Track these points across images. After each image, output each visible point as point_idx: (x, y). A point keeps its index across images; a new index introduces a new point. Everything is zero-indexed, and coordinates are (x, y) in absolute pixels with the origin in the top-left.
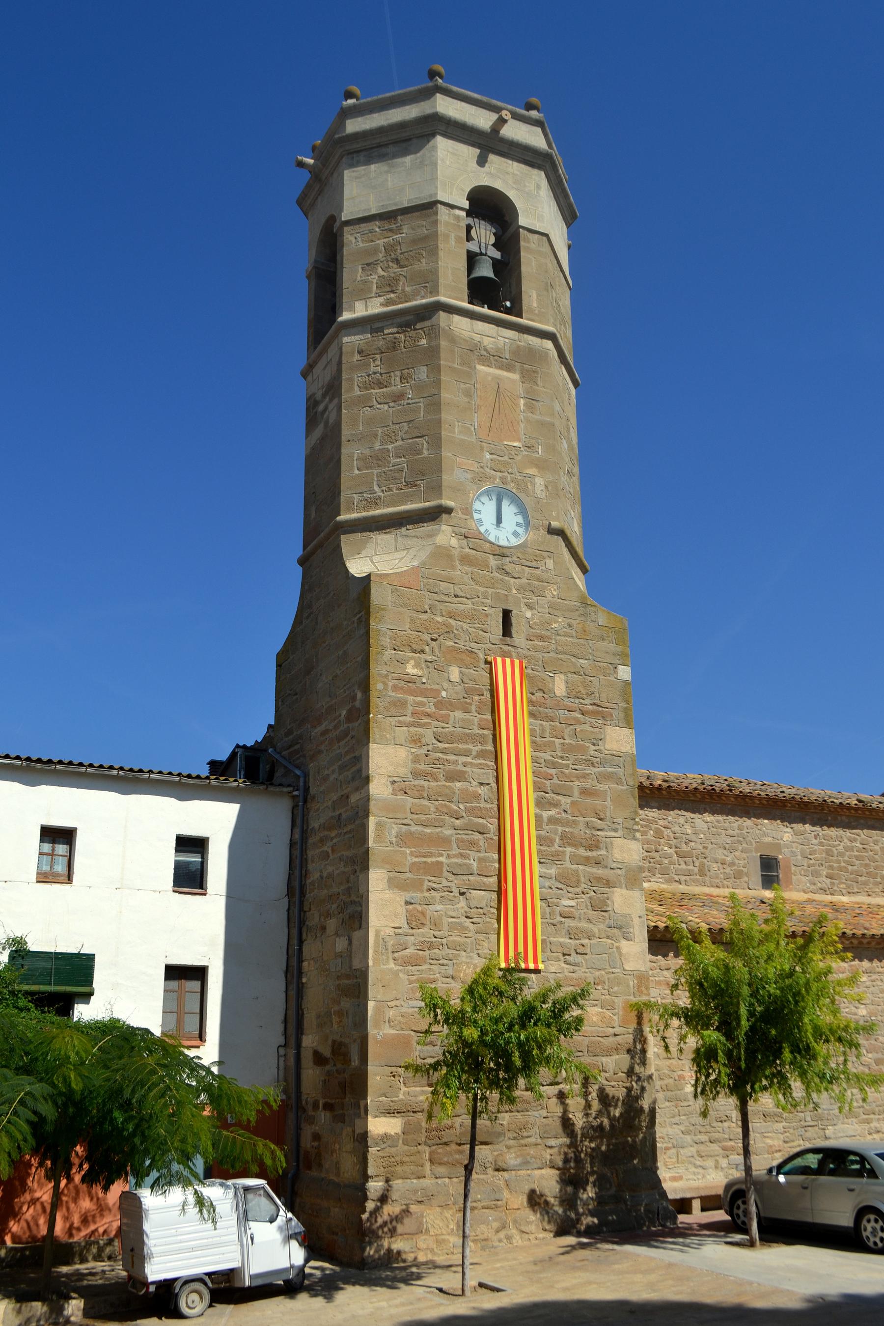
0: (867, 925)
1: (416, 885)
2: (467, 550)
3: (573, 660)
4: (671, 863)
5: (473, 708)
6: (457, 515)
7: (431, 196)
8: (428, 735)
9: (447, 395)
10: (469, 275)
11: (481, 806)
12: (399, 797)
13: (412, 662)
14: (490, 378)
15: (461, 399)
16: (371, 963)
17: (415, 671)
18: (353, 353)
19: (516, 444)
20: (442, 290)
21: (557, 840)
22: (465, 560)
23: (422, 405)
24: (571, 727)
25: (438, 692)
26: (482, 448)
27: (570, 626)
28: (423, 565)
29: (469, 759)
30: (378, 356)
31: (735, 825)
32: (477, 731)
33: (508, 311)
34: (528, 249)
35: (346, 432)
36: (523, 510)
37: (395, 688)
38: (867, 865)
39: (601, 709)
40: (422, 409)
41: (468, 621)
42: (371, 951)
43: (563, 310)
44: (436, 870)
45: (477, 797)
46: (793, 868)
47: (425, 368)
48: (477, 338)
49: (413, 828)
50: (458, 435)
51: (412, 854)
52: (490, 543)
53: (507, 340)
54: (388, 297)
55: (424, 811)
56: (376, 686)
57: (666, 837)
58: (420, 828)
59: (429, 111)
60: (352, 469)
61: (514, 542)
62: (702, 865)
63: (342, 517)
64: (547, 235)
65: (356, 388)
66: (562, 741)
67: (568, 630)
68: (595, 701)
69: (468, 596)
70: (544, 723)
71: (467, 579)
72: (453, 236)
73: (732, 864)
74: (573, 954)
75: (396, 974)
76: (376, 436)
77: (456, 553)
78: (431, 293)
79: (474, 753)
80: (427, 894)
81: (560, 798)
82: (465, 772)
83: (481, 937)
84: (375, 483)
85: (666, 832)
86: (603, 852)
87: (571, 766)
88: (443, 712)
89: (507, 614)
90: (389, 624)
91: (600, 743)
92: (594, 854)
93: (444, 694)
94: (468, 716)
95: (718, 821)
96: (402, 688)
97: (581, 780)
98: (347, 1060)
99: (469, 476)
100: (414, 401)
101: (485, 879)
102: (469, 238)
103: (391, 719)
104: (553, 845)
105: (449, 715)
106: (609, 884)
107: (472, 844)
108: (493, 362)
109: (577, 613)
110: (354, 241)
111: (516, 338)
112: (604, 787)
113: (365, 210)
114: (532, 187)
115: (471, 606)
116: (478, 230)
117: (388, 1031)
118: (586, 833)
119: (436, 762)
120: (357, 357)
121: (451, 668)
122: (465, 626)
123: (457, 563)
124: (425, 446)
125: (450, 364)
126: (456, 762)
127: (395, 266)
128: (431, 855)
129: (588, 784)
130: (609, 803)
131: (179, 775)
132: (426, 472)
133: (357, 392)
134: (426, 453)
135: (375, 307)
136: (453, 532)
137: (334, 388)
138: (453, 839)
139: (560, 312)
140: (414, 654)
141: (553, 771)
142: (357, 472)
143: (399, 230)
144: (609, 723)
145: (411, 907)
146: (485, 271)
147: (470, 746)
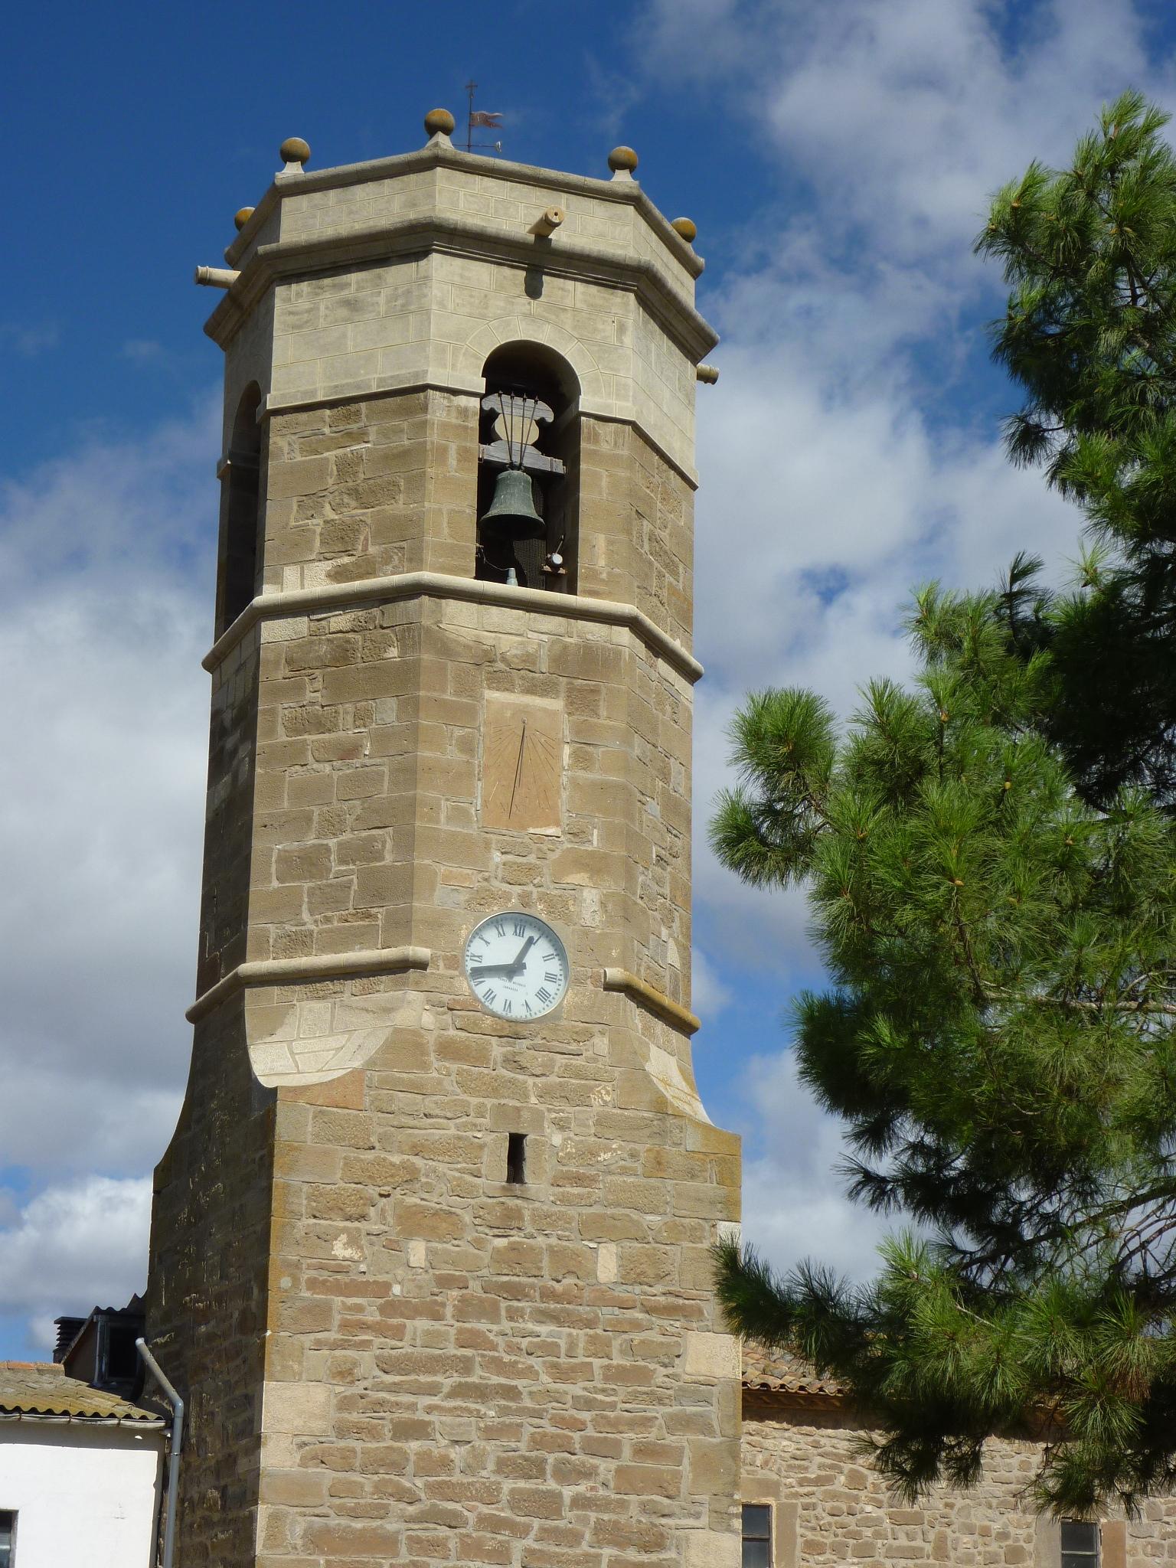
2: (452, 1032)
3: (635, 1215)
4: (878, 1535)
5: (449, 1311)
7: (416, 375)
9: (427, 754)
11: (454, 1479)
12: (310, 1470)
13: (344, 1238)
14: (508, 714)
15: (453, 755)
17: (348, 1253)
18: (277, 663)
19: (551, 831)
20: (429, 557)
21: (588, 1536)
22: (448, 1050)
23: (386, 769)
24: (625, 1336)
25: (387, 1286)
26: (487, 845)
27: (632, 1156)
28: (371, 1064)
29: (435, 1400)
30: (317, 672)
31: (1015, 1461)
33: (552, 581)
35: (261, 811)
37: (312, 1284)
39: (681, 1301)
40: (386, 778)
41: (447, 1159)
45: (445, 1463)
46: (1129, 1542)
47: (392, 703)
48: (489, 639)
49: (334, 1522)
52: (494, 1015)
53: (545, 637)
54: (340, 561)
55: (352, 1490)
56: (280, 1282)
57: (870, 1487)
58: (344, 1521)
61: (540, 1009)
62: (942, 1539)
63: (247, 968)
65: (281, 730)
66: (606, 1361)
67: (629, 1163)
68: (672, 1289)
69: (449, 1115)
70: (574, 1332)
71: (449, 1084)
72: (453, 448)
73: (1003, 1536)
77: (431, 1039)
78: (410, 560)
79: (446, 1390)
82: (429, 1423)
84: (305, 906)
86: (671, 1554)
87: (621, 1406)
88: (394, 1321)
89: (516, 1143)
91: (677, 1361)
93: (396, 1289)
94: (438, 1325)
96: (324, 1282)
97: (638, 1429)
99: (463, 897)
100: (373, 761)
102: (487, 435)
103: (302, 1337)
104: (579, 1543)
105: (405, 1326)
108: (518, 682)
109: (647, 1132)
110: (286, 449)
111: (562, 630)
113: (306, 393)
114: (610, 330)
115: (453, 1131)
116: (508, 418)
118: (640, 1522)
119: (377, 1408)
120: (284, 671)
121: (412, 1244)
122: (442, 1168)
123: (433, 1057)
124: (389, 845)
125: (435, 694)
126: (412, 1407)
127: (353, 504)
129: (652, 1435)
130: (686, 1467)
132: (388, 892)
133: (282, 737)
134: (389, 858)
136: (428, 1002)
138: (403, 1538)
140: (348, 1224)
141: (586, 1416)
142: (275, 884)
143: (360, 436)
144: (695, 1325)
146: (516, 501)
147: (439, 1378)
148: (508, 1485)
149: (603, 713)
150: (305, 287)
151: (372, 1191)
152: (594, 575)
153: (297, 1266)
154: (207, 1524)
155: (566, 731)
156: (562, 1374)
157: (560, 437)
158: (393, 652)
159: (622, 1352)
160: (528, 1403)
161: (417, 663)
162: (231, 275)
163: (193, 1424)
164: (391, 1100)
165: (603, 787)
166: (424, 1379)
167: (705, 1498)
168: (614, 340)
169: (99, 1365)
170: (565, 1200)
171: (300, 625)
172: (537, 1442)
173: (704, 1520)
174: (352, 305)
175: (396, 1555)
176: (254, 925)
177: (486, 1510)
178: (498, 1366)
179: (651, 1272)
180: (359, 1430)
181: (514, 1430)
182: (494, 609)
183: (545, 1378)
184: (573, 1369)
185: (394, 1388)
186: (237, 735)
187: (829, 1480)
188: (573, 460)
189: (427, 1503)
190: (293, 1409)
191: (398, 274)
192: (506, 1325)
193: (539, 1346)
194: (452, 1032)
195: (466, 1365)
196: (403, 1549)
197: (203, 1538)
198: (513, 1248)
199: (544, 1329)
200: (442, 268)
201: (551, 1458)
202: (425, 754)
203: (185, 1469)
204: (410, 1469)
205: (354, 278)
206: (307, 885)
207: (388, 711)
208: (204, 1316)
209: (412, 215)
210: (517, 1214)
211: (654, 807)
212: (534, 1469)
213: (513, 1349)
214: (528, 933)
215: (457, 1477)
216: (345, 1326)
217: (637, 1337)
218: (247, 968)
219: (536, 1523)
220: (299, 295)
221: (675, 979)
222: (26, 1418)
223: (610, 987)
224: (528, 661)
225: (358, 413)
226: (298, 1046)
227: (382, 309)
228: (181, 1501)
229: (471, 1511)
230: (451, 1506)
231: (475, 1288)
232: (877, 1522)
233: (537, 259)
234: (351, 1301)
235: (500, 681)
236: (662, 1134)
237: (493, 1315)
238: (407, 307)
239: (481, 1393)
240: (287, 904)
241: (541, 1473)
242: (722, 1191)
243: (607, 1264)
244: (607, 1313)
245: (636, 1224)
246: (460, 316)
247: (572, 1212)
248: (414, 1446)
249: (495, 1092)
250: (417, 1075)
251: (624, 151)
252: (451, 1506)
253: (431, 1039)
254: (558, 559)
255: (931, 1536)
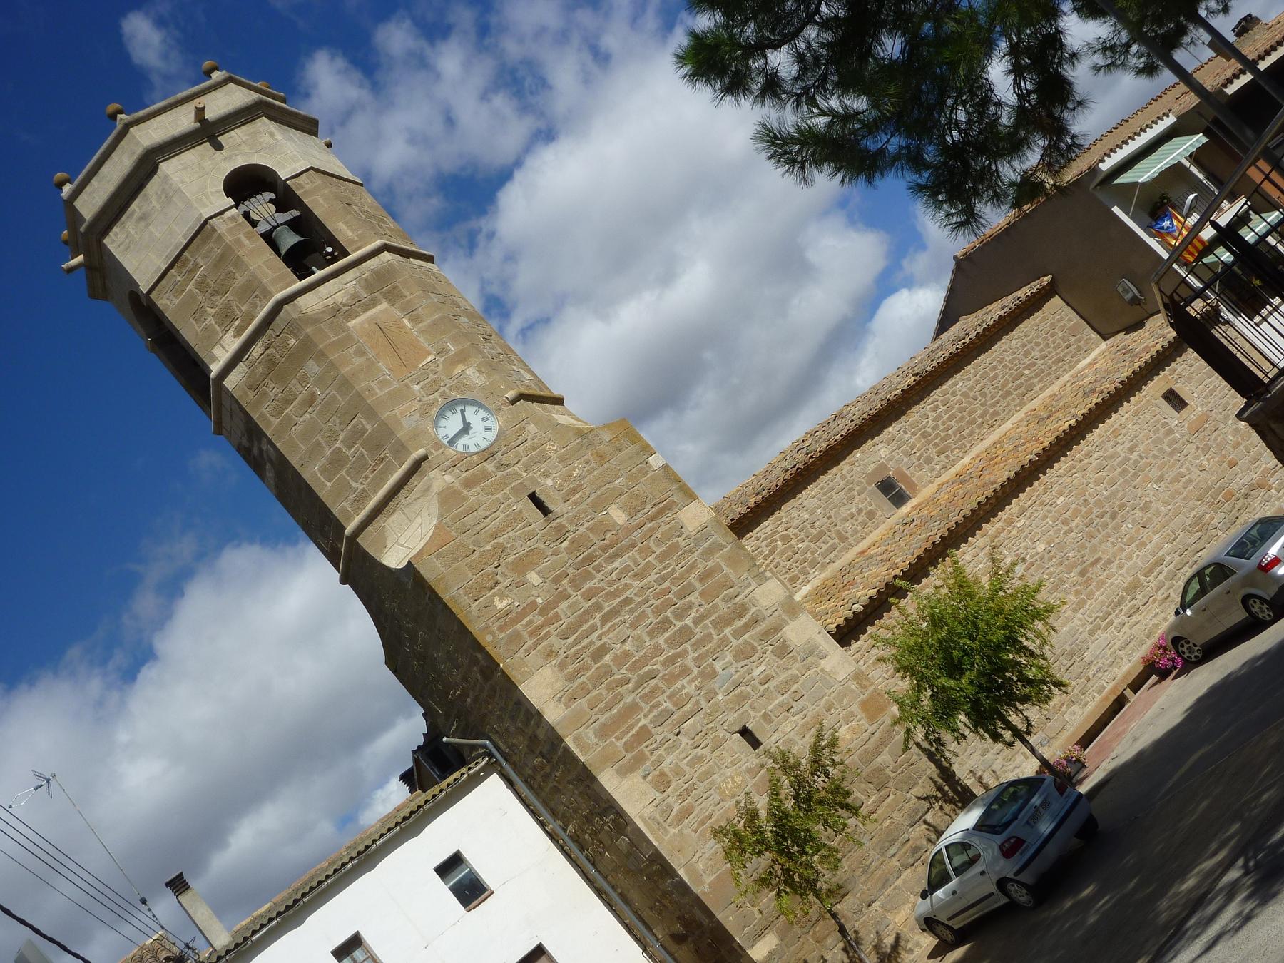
0: (992, 478)
1: (639, 760)
2: (464, 475)
3: (611, 486)
4: (813, 553)
5: (570, 591)
6: (434, 454)
7: (198, 219)
8: (554, 640)
10: (279, 254)
13: (497, 598)
15: (358, 361)
16: (656, 844)
17: (504, 603)
19: (429, 359)
20: (272, 289)
22: (469, 484)
25: (534, 602)
26: (407, 386)
28: (441, 517)
29: (599, 632)
32: (586, 605)
34: (307, 193)
35: (294, 461)
36: (479, 405)
37: (501, 629)
38: (962, 418)
42: (649, 835)
43: (372, 212)
44: (644, 734)
45: (627, 654)
46: (908, 472)
47: (311, 362)
48: (329, 302)
49: (603, 719)
50: (381, 393)
51: (618, 739)
55: (599, 699)
56: (486, 640)
58: (607, 715)
59: (139, 151)
60: (324, 485)
61: (492, 436)
62: (838, 533)
63: (349, 530)
64: (311, 168)
65: (272, 419)
71: (482, 497)
73: (860, 511)
74: (794, 704)
75: (681, 833)
76: (319, 444)
77: (457, 485)
80: (653, 758)
81: (688, 599)
83: (717, 753)
85: (790, 532)
86: (753, 610)
89: (533, 497)
90: (455, 590)
92: (747, 617)
93: (539, 600)
94: (571, 600)
95: (822, 488)
98: (700, 925)
99: (417, 416)
101: (685, 709)
102: (254, 224)
106: (777, 629)
107: (655, 691)
112: (715, 560)
114: (266, 139)
115: (502, 516)
117: (709, 879)
121: (528, 576)
122: (511, 534)
123: (465, 492)
126: (592, 642)
128: (632, 727)
129: (701, 569)
131: (397, 824)
132: (382, 441)
133: (276, 421)
134: (369, 428)
135: (232, 344)
137: (253, 431)
138: (638, 700)
139: (371, 216)
141: (667, 584)
142: (329, 484)
143: (197, 266)
145: (650, 777)
146: (289, 240)
147: (592, 622)
148: (661, 640)
149: (407, 294)
150: (115, 229)
151: (491, 569)
152: (351, 242)
153: (487, 627)
154: (546, 777)
155: (398, 313)
156: (640, 576)
157: (285, 198)
158: (292, 341)
159: (658, 546)
160: (638, 599)
161: (307, 336)
162: (81, 258)
163: (501, 744)
164: (463, 524)
165: (435, 323)
166: (585, 627)
167: (746, 575)
168: (272, 141)
169: (435, 774)
170: (576, 504)
171: (241, 367)
172: (657, 612)
173: (754, 585)
174: (144, 217)
175: (642, 710)
176: (336, 511)
177: (661, 658)
178: (612, 595)
179: (639, 503)
180: (578, 672)
181: (643, 616)
182: (321, 288)
183: (636, 583)
184: (644, 569)
185: (577, 642)
186: (255, 443)
187: (775, 548)
188: (299, 204)
189: (635, 677)
190: (541, 688)
191: (153, 186)
192: (599, 576)
193: (621, 572)
194: (464, 475)
195: (598, 607)
196: (643, 705)
197: (551, 785)
198: (572, 541)
199: (617, 564)
200: (169, 168)
201: (669, 614)
202: (345, 370)
203: (514, 766)
204: (614, 669)
205: (134, 206)
206: (343, 473)
207: (312, 367)
208: (465, 694)
209: (135, 157)
210: (562, 526)
211: (463, 320)
212: (666, 624)
213: (611, 583)
214: (458, 409)
215: (637, 656)
216: (531, 634)
217: (658, 534)
218: (349, 530)
219: (687, 645)
220: (116, 235)
221: (536, 384)
222: (426, 807)
223: (513, 402)
224: (356, 299)
225: (186, 259)
226: (402, 541)
227: (158, 207)
228: (525, 781)
229: (656, 664)
230: (646, 669)
231: (571, 571)
232: (808, 548)
233: (208, 133)
234: (524, 622)
235: (351, 315)
236: (591, 444)
237: (589, 576)
238: (168, 197)
239: (615, 612)
240: (343, 487)
241: (671, 624)
242: (637, 446)
243: (618, 515)
244: (637, 535)
245: (615, 489)
246: (196, 183)
247: (583, 506)
248: (607, 658)
249: (505, 485)
250: (465, 505)
251: (207, 64)
252: (646, 669)
253: (457, 485)
254: (329, 249)
255: (833, 535)
